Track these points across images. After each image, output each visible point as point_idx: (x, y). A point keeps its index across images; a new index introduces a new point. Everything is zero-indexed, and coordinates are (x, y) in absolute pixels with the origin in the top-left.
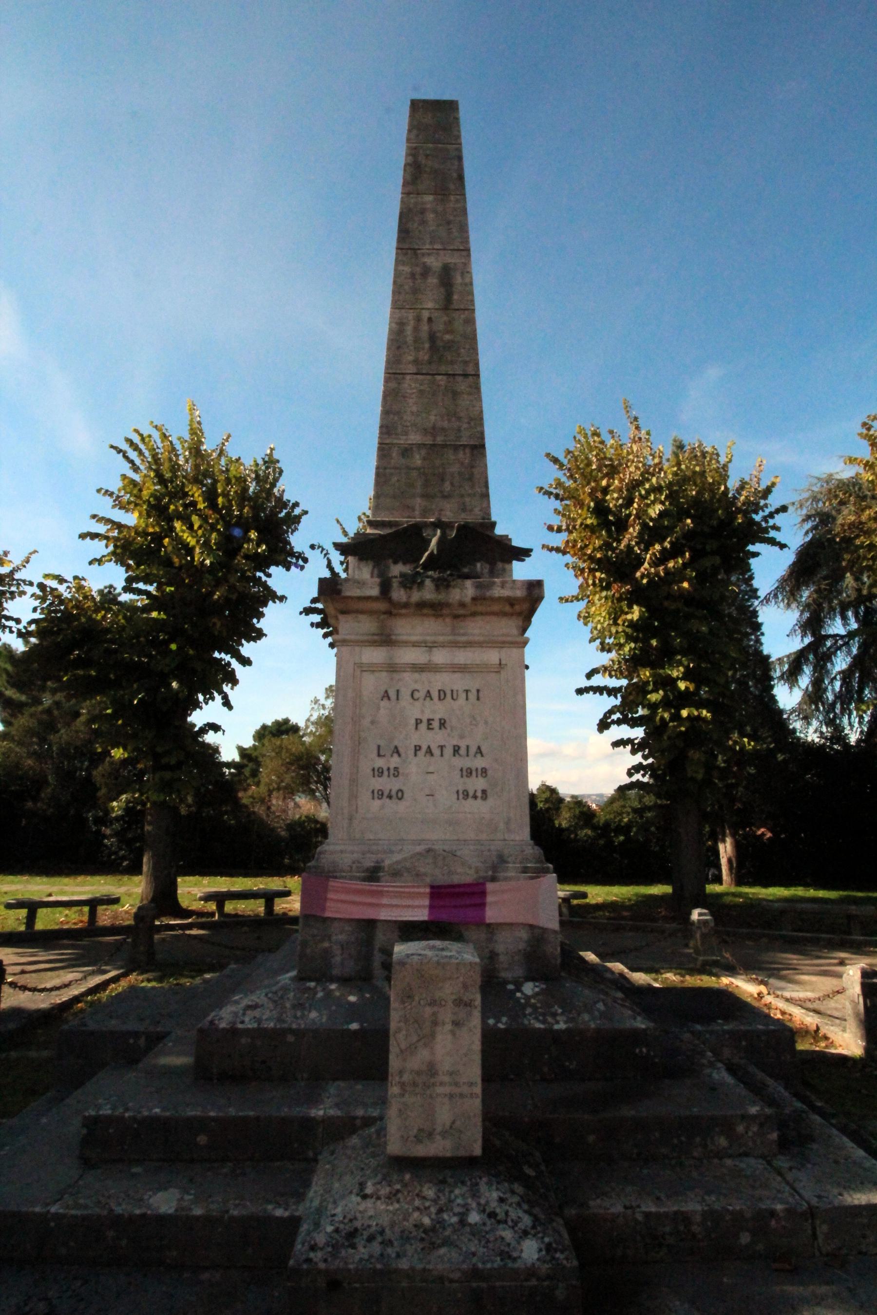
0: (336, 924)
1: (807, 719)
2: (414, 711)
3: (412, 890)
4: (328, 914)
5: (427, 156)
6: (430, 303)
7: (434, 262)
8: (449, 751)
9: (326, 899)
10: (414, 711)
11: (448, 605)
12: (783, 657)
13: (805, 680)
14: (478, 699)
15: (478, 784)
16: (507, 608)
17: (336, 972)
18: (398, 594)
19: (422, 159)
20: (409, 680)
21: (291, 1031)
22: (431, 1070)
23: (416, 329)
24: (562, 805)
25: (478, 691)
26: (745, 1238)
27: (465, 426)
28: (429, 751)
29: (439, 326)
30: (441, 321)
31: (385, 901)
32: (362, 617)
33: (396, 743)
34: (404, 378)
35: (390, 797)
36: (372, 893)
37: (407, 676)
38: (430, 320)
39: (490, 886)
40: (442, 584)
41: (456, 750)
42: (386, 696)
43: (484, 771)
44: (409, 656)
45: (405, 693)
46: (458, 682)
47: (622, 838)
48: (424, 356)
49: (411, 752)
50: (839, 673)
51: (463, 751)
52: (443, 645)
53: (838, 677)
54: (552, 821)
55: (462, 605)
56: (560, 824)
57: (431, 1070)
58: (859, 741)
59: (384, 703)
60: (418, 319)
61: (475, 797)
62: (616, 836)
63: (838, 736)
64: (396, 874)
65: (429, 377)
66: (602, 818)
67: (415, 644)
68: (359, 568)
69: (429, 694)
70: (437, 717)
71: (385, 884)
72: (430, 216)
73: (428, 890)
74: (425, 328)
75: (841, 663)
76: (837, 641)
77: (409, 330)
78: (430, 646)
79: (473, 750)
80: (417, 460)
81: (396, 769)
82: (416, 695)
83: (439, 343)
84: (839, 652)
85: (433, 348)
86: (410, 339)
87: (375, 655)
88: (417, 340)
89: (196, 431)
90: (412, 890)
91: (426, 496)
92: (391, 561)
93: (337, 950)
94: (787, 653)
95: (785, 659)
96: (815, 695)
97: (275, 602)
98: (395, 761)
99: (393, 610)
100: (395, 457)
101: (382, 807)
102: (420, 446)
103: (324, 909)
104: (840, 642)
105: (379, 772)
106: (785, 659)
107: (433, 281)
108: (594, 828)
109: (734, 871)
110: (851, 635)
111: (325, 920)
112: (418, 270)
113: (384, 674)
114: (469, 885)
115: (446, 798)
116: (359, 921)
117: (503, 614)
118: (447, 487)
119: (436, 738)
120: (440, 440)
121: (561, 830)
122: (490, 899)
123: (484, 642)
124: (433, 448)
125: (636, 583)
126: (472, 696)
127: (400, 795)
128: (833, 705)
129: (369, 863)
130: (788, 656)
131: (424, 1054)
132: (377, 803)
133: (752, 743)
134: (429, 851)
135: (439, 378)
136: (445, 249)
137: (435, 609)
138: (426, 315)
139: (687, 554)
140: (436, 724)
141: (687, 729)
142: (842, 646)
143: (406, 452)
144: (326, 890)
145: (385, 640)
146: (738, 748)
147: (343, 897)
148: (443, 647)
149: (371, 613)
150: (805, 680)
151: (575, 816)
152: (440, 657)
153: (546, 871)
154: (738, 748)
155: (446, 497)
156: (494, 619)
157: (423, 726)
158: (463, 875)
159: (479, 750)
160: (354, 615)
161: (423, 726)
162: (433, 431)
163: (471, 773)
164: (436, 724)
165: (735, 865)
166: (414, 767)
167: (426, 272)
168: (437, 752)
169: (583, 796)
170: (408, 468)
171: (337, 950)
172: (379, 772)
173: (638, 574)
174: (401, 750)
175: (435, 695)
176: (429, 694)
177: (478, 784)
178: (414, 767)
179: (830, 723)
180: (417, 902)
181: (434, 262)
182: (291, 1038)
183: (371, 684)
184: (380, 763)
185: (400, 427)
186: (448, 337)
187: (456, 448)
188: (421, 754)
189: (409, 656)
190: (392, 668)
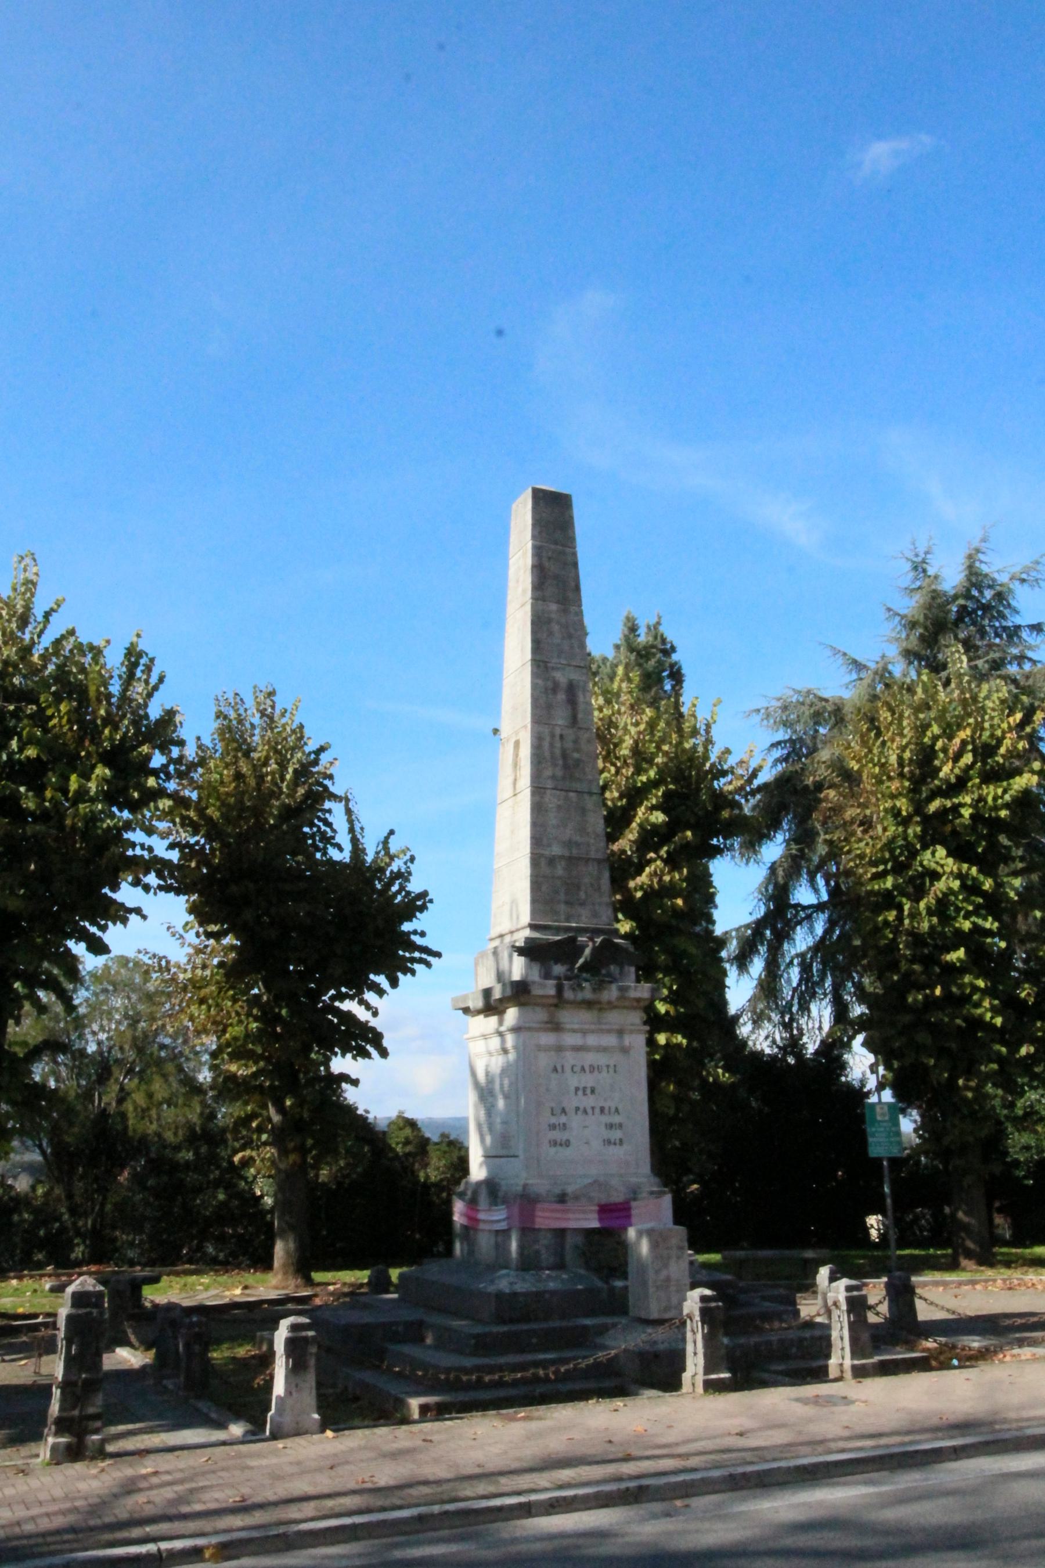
1: (757, 1022)
2: (573, 1081)
4: (537, 1227)
5: (549, 558)
6: (561, 718)
7: (561, 677)
8: (597, 1111)
10: (573, 1081)
11: (599, 1003)
12: (731, 930)
13: (757, 966)
14: (615, 1071)
15: (617, 1134)
16: (635, 1004)
17: (544, 1264)
18: (568, 994)
19: (546, 564)
20: (570, 1059)
22: (668, 1279)
23: (552, 745)
24: (429, 1148)
26: (794, 1350)
27: (592, 841)
28: (585, 1112)
29: (569, 745)
30: (570, 734)
31: (571, 1216)
34: (545, 793)
35: (561, 1145)
36: (564, 1211)
38: (561, 737)
39: (633, 1204)
40: (599, 987)
41: (602, 1110)
42: (555, 1070)
43: (620, 1126)
44: (570, 1039)
45: (568, 1069)
46: (602, 1059)
48: (559, 773)
50: (797, 955)
51: (606, 1111)
52: (593, 1032)
53: (796, 962)
54: (414, 1174)
55: (609, 1003)
56: (427, 1177)
57: (668, 1279)
58: (817, 1053)
59: (554, 1076)
60: (553, 736)
61: (615, 1144)
63: (793, 1045)
64: (577, 1198)
65: (563, 793)
67: (574, 1031)
68: (531, 968)
69: (583, 1069)
70: (589, 1085)
71: (570, 1205)
72: (556, 628)
73: (597, 1208)
74: (558, 745)
75: (802, 940)
76: (797, 912)
77: (546, 744)
78: (584, 1032)
79: (613, 1110)
80: (560, 871)
81: (564, 1124)
82: (575, 1069)
83: (570, 762)
84: (798, 927)
85: (566, 767)
86: (547, 754)
87: (547, 1039)
91: (567, 903)
92: (552, 962)
93: (543, 1251)
94: (737, 926)
95: (734, 934)
96: (769, 987)
97: (413, 972)
98: (563, 1119)
99: (559, 1001)
100: (545, 870)
101: (557, 1153)
102: (562, 857)
103: (533, 1222)
104: (802, 914)
105: (553, 1127)
106: (734, 934)
107: (561, 696)
110: (820, 907)
111: (534, 1230)
112: (550, 684)
113: (553, 1053)
114: (621, 1204)
115: (596, 1144)
116: (550, 1230)
117: (635, 1008)
118: (582, 895)
119: (589, 1101)
120: (575, 852)
121: (426, 1186)
122: (634, 1212)
124: (571, 861)
125: (628, 894)
126: (611, 1070)
127: (567, 1144)
128: (790, 1004)
129: (557, 1191)
130: (737, 930)
131: (664, 1274)
132: (553, 1150)
133: (727, 1075)
134: (595, 1182)
135: (572, 794)
136: (569, 665)
137: (589, 1004)
138: (558, 731)
139: (685, 871)
140: (588, 1091)
141: (662, 1058)
142: (803, 919)
143: (552, 861)
145: (555, 1027)
146: (711, 1079)
147: (547, 1214)
149: (543, 1005)
150: (757, 966)
151: (452, 1164)
152: (592, 1040)
153: (664, 1193)
154: (711, 1079)
155: (582, 904)
156: (625, 1011)
157: (580, 1093)
158: (617, 1197)
159: (617, 1110)
161: (580, 1093)
162: (569, 844)
164: (588, 1091)
166: (575, 1121)
167: (555, 688)
168: (590, 1111)
170: (553, 877)
171: (543, 1251)
172: (553, 1127)
173: (632, 884)
174: (567, 1110)
175: (587, 1069)
176: (583, 1069)
177: (617, 1134)
178: (575, 1121)
179: (787, 1026)
181: (561, 677)
182: (547, 1296)
183: (544, 1061)
184: (553, 1120)
186: (576, 755)
187: (587, 860)
188: (579, 1113)
190: (559, 1049)
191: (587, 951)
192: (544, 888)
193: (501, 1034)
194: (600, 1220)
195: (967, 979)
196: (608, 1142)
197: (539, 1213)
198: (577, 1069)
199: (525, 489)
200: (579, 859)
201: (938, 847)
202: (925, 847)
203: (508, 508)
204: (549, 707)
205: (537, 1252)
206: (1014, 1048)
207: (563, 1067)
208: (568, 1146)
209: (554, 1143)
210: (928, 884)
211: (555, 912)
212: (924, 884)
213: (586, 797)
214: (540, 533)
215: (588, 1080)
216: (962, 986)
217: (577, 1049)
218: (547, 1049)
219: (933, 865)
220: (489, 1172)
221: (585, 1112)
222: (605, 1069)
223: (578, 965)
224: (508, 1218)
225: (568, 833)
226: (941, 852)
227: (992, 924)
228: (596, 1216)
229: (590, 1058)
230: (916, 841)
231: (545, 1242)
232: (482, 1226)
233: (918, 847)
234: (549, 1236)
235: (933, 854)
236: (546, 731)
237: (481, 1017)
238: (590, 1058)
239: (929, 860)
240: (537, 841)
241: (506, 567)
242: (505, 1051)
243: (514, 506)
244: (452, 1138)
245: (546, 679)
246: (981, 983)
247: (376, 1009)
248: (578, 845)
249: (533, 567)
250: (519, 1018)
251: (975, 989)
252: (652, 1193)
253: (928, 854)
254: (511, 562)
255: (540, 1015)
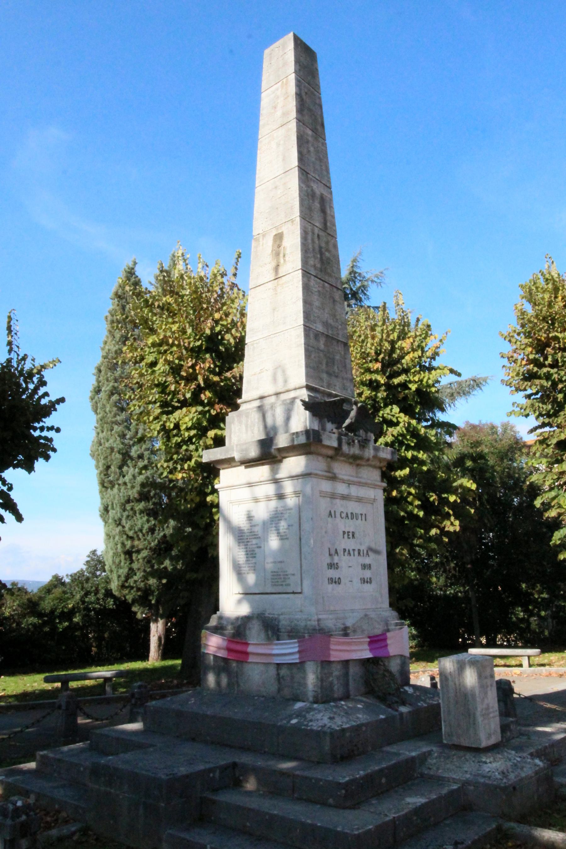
0: (334, 665)
3: (362, 640)
4: (332, 659)
9: (329, 649)
14: (366, 520)
21: (363, 725)
22: (488, 705)
25: (365, 515)
32: (320, 458)
33: (336, 547)
36: (349, 644)
37: (338, 502)
45: (338, 515)
47: (67, 624)
49: (342, 553)
59: (330, 519)
62: (60, 623)
65: (322, 282)
66: (47, 605)
70: (351, 530)
85: (321, 260)
88: (314, 250)
89: (481, 389)
90: (362, 640)
92: (326, 420)
93: (335, 682)
100: (312, 341)
103: (329, 655)
107: (317, 205)
108: (40, 615)
109: (161, 648)
113: (329, 499)
119: (350, 544)
122: (389, 642)
123: (371, 484)
132: (330, 586)
135: (326, 284)
144: (329, 643)
148: (354, 484)
156: (371, 469)
160: (314, 456)
163: (365, 567)
165: (163, 642)
168: (352, 552)
169: (25, 583)
171: (335, 682)
178: (343, 560)
180: (361, 647)
185: (312, 316)
189: (341, 489)
191: (353, 414)
192: (313, 356)
193: (276, 481)
194: (371, 650)
195: (404, 487)
196: (364, 581)
197: (332, 647)
198: (344, 515)
199: (289, 32)
200: (333, 338)
201: (394, 406)
202: (386, 406)
203: (263, 52)
204: (310, 209)
205: (331, 683)
206: (427, 530)
207: (335, 512)
208: (339, 584)
209: (331, 581)
210: (385, 429)
211: (321, 379)
212: (382, 429)
213: (335, 290)
214: (300, 70)
215: (350, 525)
216: (400, 492)
217: (345, 497)
218: (323, 494)
219: (389, 417)
220: (252, 606)
221: (349, 554)
222: (360, 517)
223: (344, 425)
224: (299, 652)
225: (326, 316)
226: (396, 409)
227: (423, 455)
228: (366, 647)
229: (353, 507)
230: (381, 401)
231: (336, 673)
232: (251, 659)
233: (382, 405)
234: (339, 667)
235: (391, 410)
236: (309, 228)
237: (242, 468)
238: (353, 507)
239: (388, 414)
240: (307, 315)
241: (258, 101)
242: (280, 496)
243: (267, 52)
244: (19, 586)
245: (308, 186)
246: (413, 491)
247: (11, 485)
248: (332, 327)
249: (296, 94)
250: (307, 466)
251: (410, 494)
252: (397, 624)
253: (388, 410)
254: (263, 95)
255: (320, 465)
